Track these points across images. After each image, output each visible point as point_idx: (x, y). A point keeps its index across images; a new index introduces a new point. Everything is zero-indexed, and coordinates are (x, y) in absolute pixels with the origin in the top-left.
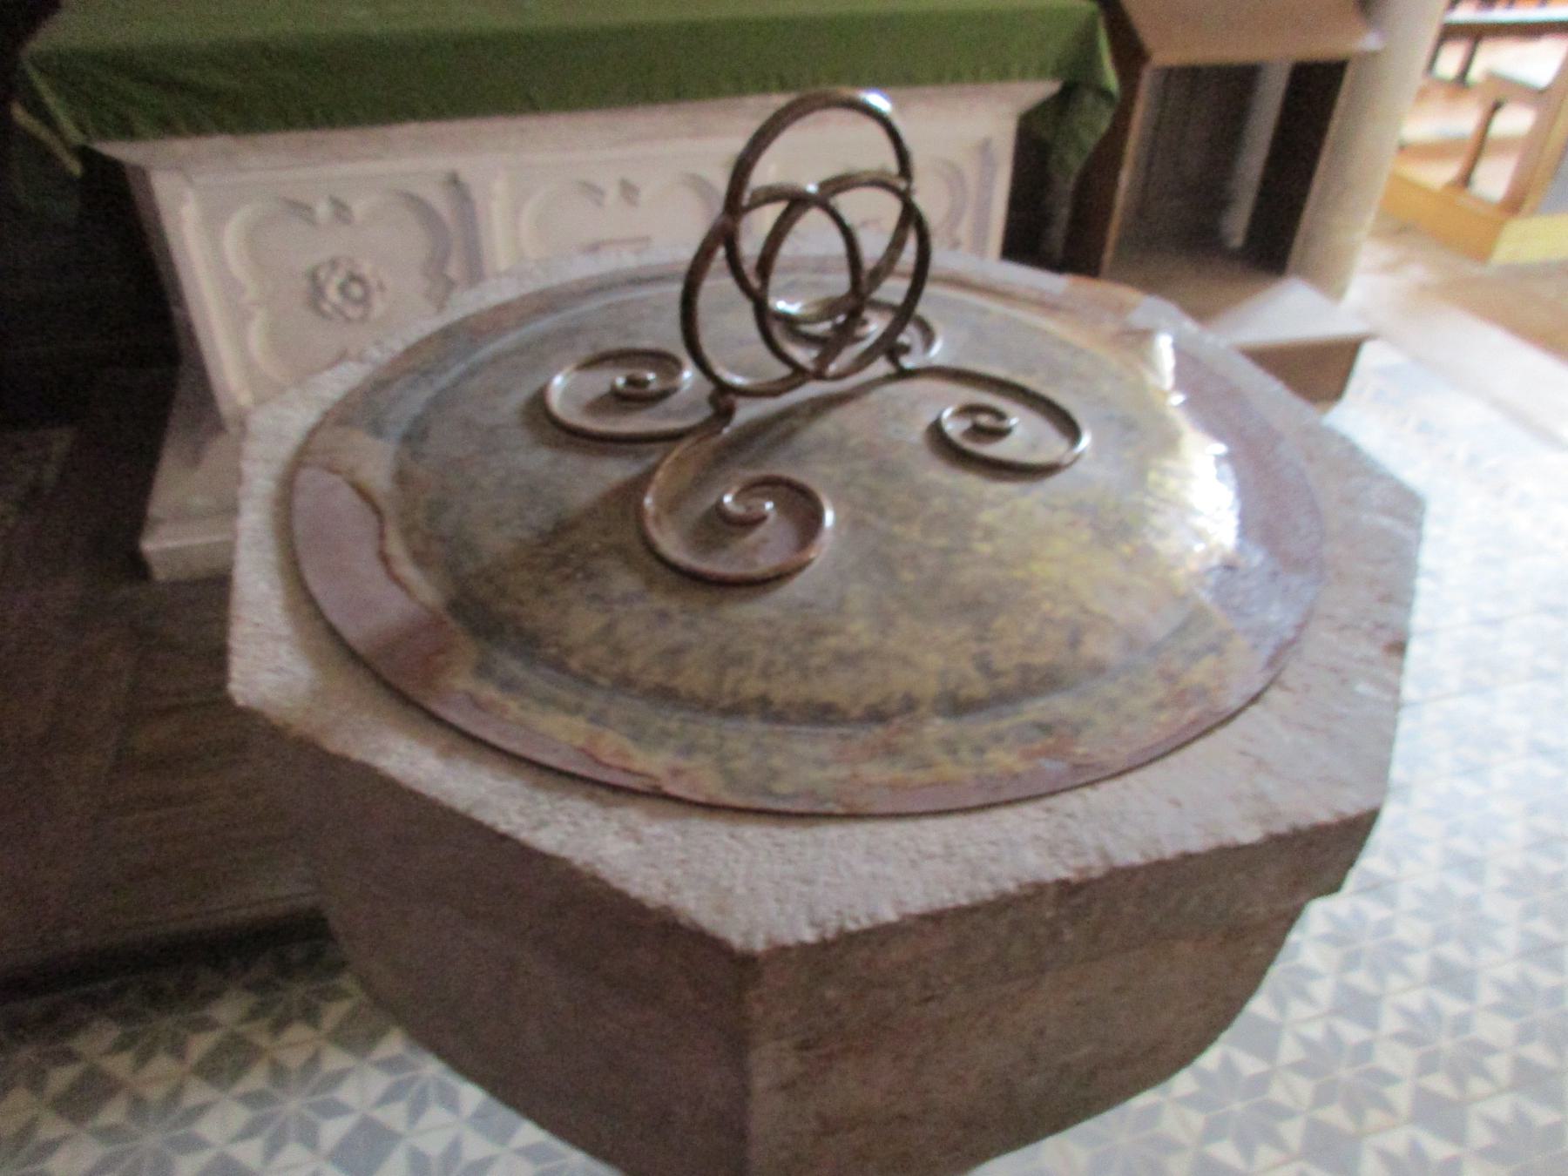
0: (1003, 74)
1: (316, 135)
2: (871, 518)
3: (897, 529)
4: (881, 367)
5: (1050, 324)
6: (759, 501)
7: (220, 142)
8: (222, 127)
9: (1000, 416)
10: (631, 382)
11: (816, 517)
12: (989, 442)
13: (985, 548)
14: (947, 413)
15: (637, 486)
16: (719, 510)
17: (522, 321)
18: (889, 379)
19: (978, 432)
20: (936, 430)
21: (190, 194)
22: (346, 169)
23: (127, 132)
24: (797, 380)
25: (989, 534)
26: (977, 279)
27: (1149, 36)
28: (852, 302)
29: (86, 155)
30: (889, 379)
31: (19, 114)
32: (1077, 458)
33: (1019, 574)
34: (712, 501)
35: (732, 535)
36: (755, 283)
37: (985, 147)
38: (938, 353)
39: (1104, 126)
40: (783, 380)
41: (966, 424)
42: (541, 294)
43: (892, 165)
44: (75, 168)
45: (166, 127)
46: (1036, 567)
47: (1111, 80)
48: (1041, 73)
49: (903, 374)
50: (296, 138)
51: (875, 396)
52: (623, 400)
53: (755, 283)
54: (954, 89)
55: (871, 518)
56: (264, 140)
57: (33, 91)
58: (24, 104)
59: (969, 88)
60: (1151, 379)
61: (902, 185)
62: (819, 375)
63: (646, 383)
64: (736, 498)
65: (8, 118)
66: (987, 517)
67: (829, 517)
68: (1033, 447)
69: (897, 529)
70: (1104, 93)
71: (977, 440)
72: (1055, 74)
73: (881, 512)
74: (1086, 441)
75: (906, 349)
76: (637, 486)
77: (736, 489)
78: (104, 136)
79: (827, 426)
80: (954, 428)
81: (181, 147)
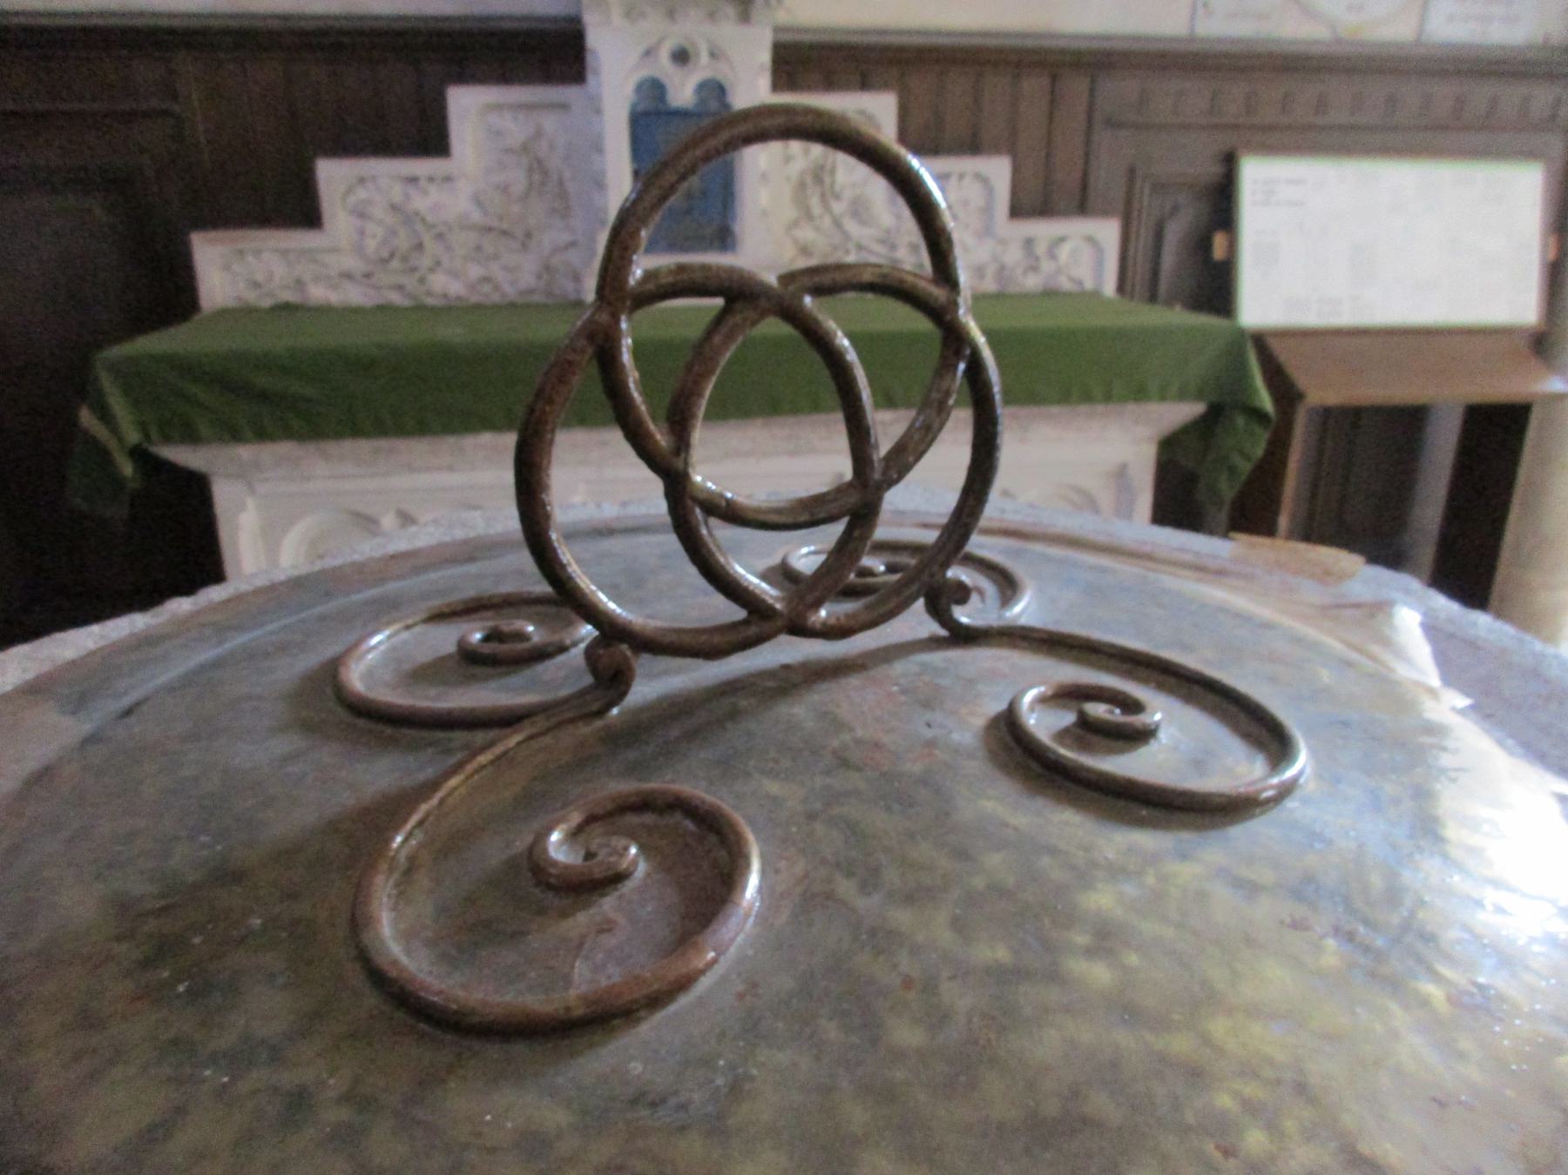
0: (1139, 394)
1: (383, 443)
2: (846, 887)
3: (901, 917)
4: (915, 622)
5: (1216, 593)
6: (622, 842)
7: (285, 448)
8: (288, 433)
9: (1133, 706)
10: (492, 636)
11: (728, 880)
12: (1111, 751)
13: (1100, 974)
14: (1030, 696)
15: (390, 810)
16: (535, 865)
17: (418, 570)
18: (934, 643)
19: (1089, 732)
20: (1008, 729)
21: (251, 503)
22: (422, 480)
23: (191, 437)
24: (753, 630)
25: (1107, 938)
26: (1102, 539)
27: (1301, 379)
28: (853, 499)
29: (140, 455)
30: (934, 643)
31: (86, 417)
32: (1286, 791)
33: (1181, 1044)
34: (521, 844)
35: (542, 911)
36: (661, 438)
37: (1121, 474)
38: (1023, 611)
39: (1259, 451)
40: (734, 626)
41: (1068, 718)
42: (466, 542)
43: (912, 258)
44: (127, 469)
45: (234, 435)
46: (1219, 1027)
47: (1266, 401)
48: (1182, 396)
49: (963, 637)
50: (364, 446)
51: (901, 668)
52: (471, 661)
53: (661, 438)
54: (1084, 408)
55: (846, 887)
56: (332, 447)
57: (100, 393)
58: (92, 408)
59: (1100, 408)
60: (1402, 671)
61: (939, 293)
62: (800, 629)
63: (521, 636)
64: (574, 835)
65: (74, 423)
66: (1102, 899)
67: (753, 881)
68: (1199, 765)
69: (901, 917)
70: (1258, 415)
71: (1083, 746)
72: (1199, 396)
73: (870, 882)
74: (1302, 762)
75: (962, 593)
76: (390, 810)
77: (576, 818)
78: (167, 439)
79: (800, 710)
80: (1043, 724)
81: (245, 452)
